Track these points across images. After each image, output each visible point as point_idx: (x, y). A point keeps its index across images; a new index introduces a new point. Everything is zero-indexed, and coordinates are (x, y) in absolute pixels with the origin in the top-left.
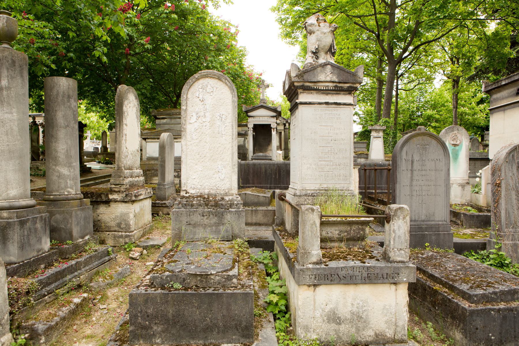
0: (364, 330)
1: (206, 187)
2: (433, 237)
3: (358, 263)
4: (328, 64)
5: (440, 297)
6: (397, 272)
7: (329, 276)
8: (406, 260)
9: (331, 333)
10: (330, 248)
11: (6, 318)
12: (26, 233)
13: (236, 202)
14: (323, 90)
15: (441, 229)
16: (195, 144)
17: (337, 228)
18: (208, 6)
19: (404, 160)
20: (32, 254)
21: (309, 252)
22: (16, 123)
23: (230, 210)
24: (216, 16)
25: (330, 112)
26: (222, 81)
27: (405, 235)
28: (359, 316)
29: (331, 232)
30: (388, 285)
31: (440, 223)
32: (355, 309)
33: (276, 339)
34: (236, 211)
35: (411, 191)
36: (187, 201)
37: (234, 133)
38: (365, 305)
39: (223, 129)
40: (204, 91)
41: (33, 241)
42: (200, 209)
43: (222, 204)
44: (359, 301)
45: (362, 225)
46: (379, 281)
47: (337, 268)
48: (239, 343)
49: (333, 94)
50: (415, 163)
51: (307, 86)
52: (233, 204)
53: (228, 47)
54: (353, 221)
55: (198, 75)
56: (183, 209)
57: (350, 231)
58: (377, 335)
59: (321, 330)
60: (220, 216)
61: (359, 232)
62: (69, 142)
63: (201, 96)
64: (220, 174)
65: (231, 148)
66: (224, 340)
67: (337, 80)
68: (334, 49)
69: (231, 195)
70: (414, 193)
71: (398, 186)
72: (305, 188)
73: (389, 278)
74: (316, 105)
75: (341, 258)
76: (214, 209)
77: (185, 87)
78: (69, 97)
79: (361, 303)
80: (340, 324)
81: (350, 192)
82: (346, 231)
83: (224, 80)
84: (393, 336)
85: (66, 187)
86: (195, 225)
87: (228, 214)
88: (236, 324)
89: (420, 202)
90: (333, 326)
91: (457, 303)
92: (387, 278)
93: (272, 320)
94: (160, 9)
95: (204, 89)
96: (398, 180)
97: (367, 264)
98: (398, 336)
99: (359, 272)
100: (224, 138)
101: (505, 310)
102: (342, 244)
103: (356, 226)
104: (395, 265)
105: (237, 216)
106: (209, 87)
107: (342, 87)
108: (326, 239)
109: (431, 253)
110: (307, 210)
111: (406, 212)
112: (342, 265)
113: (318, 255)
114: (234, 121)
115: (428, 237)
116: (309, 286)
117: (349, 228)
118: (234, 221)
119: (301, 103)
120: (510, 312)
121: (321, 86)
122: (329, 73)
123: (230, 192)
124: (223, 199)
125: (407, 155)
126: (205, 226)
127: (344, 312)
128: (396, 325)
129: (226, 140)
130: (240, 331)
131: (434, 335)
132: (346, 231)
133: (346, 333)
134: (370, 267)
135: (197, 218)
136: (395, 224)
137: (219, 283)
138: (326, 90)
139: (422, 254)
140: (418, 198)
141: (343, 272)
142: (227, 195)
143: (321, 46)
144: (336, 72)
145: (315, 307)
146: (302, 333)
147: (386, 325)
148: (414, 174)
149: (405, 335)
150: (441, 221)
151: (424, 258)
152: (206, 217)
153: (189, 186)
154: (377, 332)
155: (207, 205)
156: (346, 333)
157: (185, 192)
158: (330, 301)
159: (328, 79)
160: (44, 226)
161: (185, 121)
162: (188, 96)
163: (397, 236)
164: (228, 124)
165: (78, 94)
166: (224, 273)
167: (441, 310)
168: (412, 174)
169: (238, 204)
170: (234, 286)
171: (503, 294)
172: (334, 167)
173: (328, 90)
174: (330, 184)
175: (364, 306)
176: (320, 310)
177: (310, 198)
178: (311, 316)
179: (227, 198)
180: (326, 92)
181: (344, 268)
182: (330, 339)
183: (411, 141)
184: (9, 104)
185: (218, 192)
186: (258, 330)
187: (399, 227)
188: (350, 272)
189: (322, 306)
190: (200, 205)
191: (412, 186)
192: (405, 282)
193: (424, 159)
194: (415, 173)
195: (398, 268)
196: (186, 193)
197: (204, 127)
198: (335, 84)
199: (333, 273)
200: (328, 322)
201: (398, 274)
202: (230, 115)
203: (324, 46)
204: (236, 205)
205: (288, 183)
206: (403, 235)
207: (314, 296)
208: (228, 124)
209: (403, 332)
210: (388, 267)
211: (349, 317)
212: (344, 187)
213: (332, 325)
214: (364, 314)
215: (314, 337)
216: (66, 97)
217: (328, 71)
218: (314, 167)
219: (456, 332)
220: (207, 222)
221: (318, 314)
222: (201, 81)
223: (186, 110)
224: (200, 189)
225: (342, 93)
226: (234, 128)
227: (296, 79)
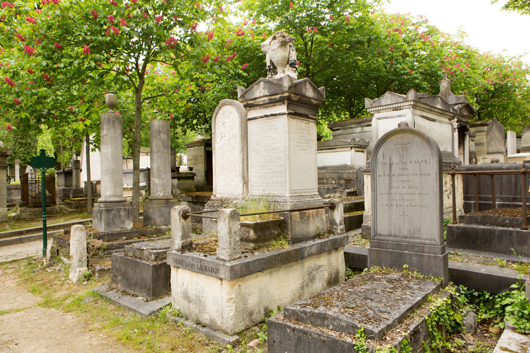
2: (414, 259)
8: (226, 260)
11: (84, 258)
12: (111, 217)
14: (262, 105)
15: (426, 249)
20: (117, 230)
22: (110, 154)
30: (216, 279)
31: (427, 242)
35: (390, 200)
41: (117, 222)
45: (248, 228)
49: (270, 106)
50: (394, 167)
58: (211, 321)
62: (159, 162)
67: (268, 94)
74: (259, 119)
78: (160, 132)
85: (157, 191)
89: (401, 213)
101: (302, 331)
115: (408, 257)
120: (305, 335)
125: (383, 157)
138: (264, 104)
140: (398, 209)
148: (393, 180)
150: (429, 239)
159: (262, 94)
160: (127, 214)
168: (390, 180)
171: (313, 316)
172: (273, 174)
173: (265, 104)
180: (265, 105)
183: (389, 141)
184: (107, 144)
193: (405, 161)
194: (394, 179)
203: (277, 61)
216: (158, 132)
225: (278, 104)
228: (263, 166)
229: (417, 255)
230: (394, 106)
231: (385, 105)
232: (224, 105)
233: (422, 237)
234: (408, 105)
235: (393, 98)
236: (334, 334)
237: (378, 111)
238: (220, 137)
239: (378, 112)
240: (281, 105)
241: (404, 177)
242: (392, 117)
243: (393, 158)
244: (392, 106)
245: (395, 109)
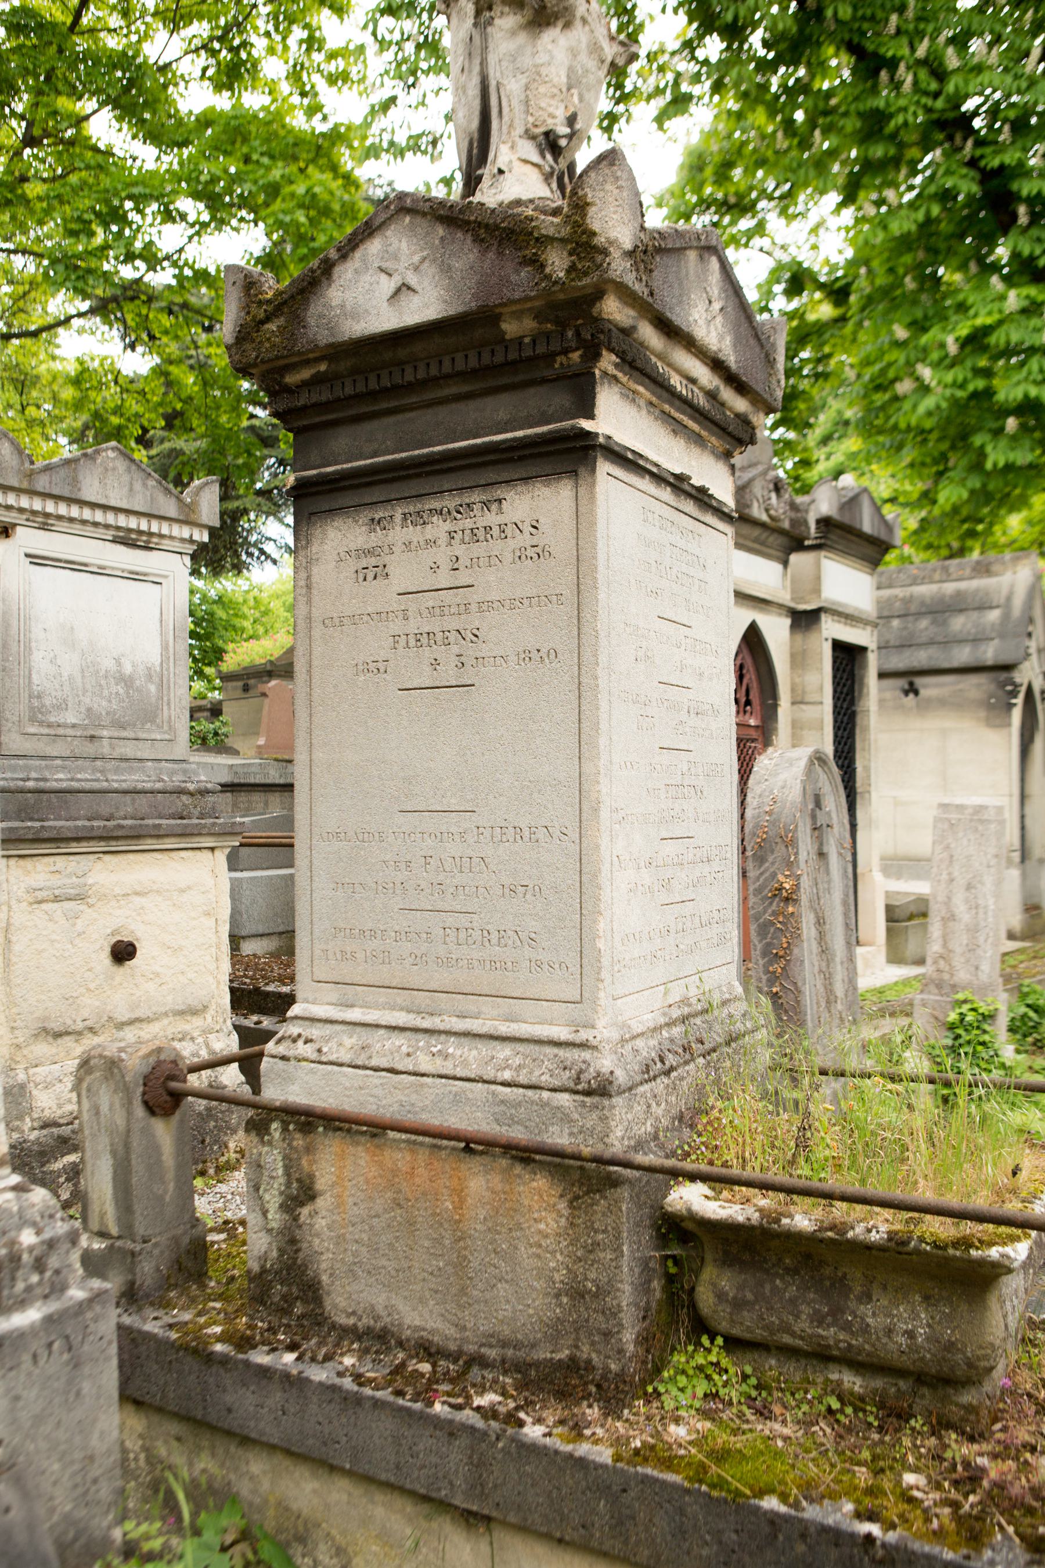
13: (28, 1238)
34: (49, 1320)
230: (133, 523)
231: (93, 506)
234: (183, 540)
235: (138, 486)
236: (87, 823)
237: (45, 522)
239: (44, 527)
242: (101, 572)
244: (122, 521)
245: (127, 539)
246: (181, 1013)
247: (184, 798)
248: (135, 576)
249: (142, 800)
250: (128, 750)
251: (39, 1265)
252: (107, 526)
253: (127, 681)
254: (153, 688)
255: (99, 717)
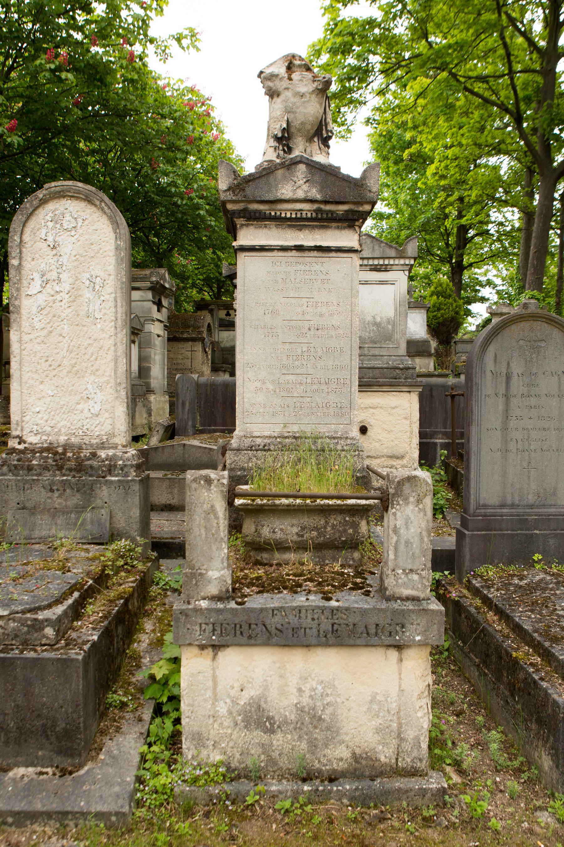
0: (326, 746)
1: (63, 431)
2: (552, 542)
3: (315, 600)
4: (300, 162)
5: (521, 675)
6: (399, 622)
7: (245, 627)
8: (422, 596)
9: (253, 752)
10: (279, 565)
13: (120, 462)
14: (291, 219)
16: (38, 340)
17: (295, 521)
18: (147, 56)
19: (489, 374)
21: (201, 574)
23: (109, 478)
24: (176, 79)
25: (307, 268)
26: (95, 205)
27: (422, 539)
28: (314, 716)
29: (281, 530)
30: (382, 650)
32: (305, 701)
33: (137, 759)
34: (119, 480)
35: (505, 441)
36: (18, 460)
37: (119, 315)
38: (329, 691)
39: (97, 308)
40: (58, 226)
42: (46, 477)
43: (91, 467)
44: (314, 684)
45: (353, 515)
46: (358, 642)
47: (261, 610)
48: (52, 766)
49: (313, 227)
50: (514, 380)
51: (255, 211)
52: (115, 466)
53: (191, 141)
54: (329, 505)
55: (44, 192)
56: (10, 477)
57: (325, 528)
58: (356, 758)
59: (231, 744)
60: (87, 492)
61: (345, 531)
63: (50, 238)
64: (91, 402)
65: (113, 348)
66: (20, 759)
67: (319, 197)
68: (327, 131)
69: (112, 448)
70: (512, 446)
71: (474, 430)
72: (251, 432)
73: (381, 633)
74: (275, 253)
75: (285, 588)
76: (74, 477)
77: (18, 218)
79: (320, 687)
80: (272, 731)
81: (349, 442)
82: (316, 529)
83: (98, 203)
84: (393, 761)
86: (33, 510)
87: (104, 488)
88: (44, 725)
89: (525, 464)
90: (258, 736)
91: (545, 690)
92: (376, 634)
93: (147, 714)
94: (38, 62)
95: (56, 223)
96: (475, 417)
97: (334, 603)
98: (406, 762)
99: (313, 619)
100: (99, 326)
102: (306, 557)
103: (339, 518)
104: (397, 605)
105: (122, 491)
106: (68, 217)
107: (332, 212)
108: (270, 544)
109: (542, 576)
110: (195, 480)
111: (424, 488)
112: (276, 604)
113: (221, 579)
114: (119, 291)
116: (202, 647)
117: (322, 522)
118: (116, 502)
119: (243, 249)
121: (286, 211)
122: (301, 182)
123: (111, 442)
124: (94, 455)
126: (54, 513)
127: (283, 703)
128: (400, 738)
129: (103, 330)
130: (53, 739)
131: (503, 759)
132: (316, 529)
133: (285, 751)
134: (338, 609)
135: (38, 495)
136: (399, 514)
137: (16, 636)
138: (296, 219)
139: (521, 578)
140: (519, 457)
141: (277, 619)
142: (104, 448)
143: (296, 124)
144: (317, 178)
145: (215, 694)
146: (188, 749)
147: (377, 738)
149: (421, 760)
151: (521, 587)
152: (56, 494)
153: (27, 428)
154: (358, 751)
155: (60, 468)
156: (285, 751)
157: (18, 440)
158: (249, 682)
159: (300, 194)
161: (18, 290)
162: (24, 237)
163: (403, 541)
164: (107, 297)
165: (236, 278)
166: (28, 615)
167: (523, 705)
169: (125, 466)
170: (48, 642)
173: (301, 219)
174: (305, 425)
175: (327, 695)
176: (228, 701)
177: (260, 453)
178: (208, 713)
179: (103, 454)
180: (297, 223)
181: (279, 609)
182: (249, 762)
183: (507, 331)
185: (87, 440)
186: (106, 740)
187: (407, 522)
188: (293, 620)
189: (233, 693)
190: (46, 468)
191: (506, 429)
192: (421, 644)
194: (514, 402)
195: (403, 613)
196: (19, 443)
197: (59, 304)
198: (315, 206)
199: (253, 621)
200: (246, 727)
201: (403, 627)
202: (112, 277)
203: (303, 123)
204: (122, 469)
205: (234, 424)
206: (416, 539)
207: (214, 669)
208: (107, 297)
209: (415, 753)
210: (380, 610)
211: (293, 717)
212: (336, 432)
213: (255, 733)
214: (327, 712)
215: (217, 757)
217: (300, 177)
218: (271, 387)
219: (543, 753)
220: (60, 504)
221: (222, 709)
222: (51, 206)
223: (19, 267)
224: (48, 435)
225: (334, 225)
226: (119, 304)
227: (229, 196)
228: (284, 366)
229: (556, 535)
230: (376, 262)
232: (60, 195)
233: (559, 503)
235: (376, 247)
238: (38, 283)
240: (344, 228)
241: (532, 399)
243: (513, 365)
244: (371, 262)
245: (376, 269)
246: (392, 457)
247: (397, 371)
248: (382, 283)
249: (377, 371)
250: (377, 352)
251: (122, 469)
252: (366, 265)
253: (376, 324)
254: (390, 327)
255: (365, 339)
